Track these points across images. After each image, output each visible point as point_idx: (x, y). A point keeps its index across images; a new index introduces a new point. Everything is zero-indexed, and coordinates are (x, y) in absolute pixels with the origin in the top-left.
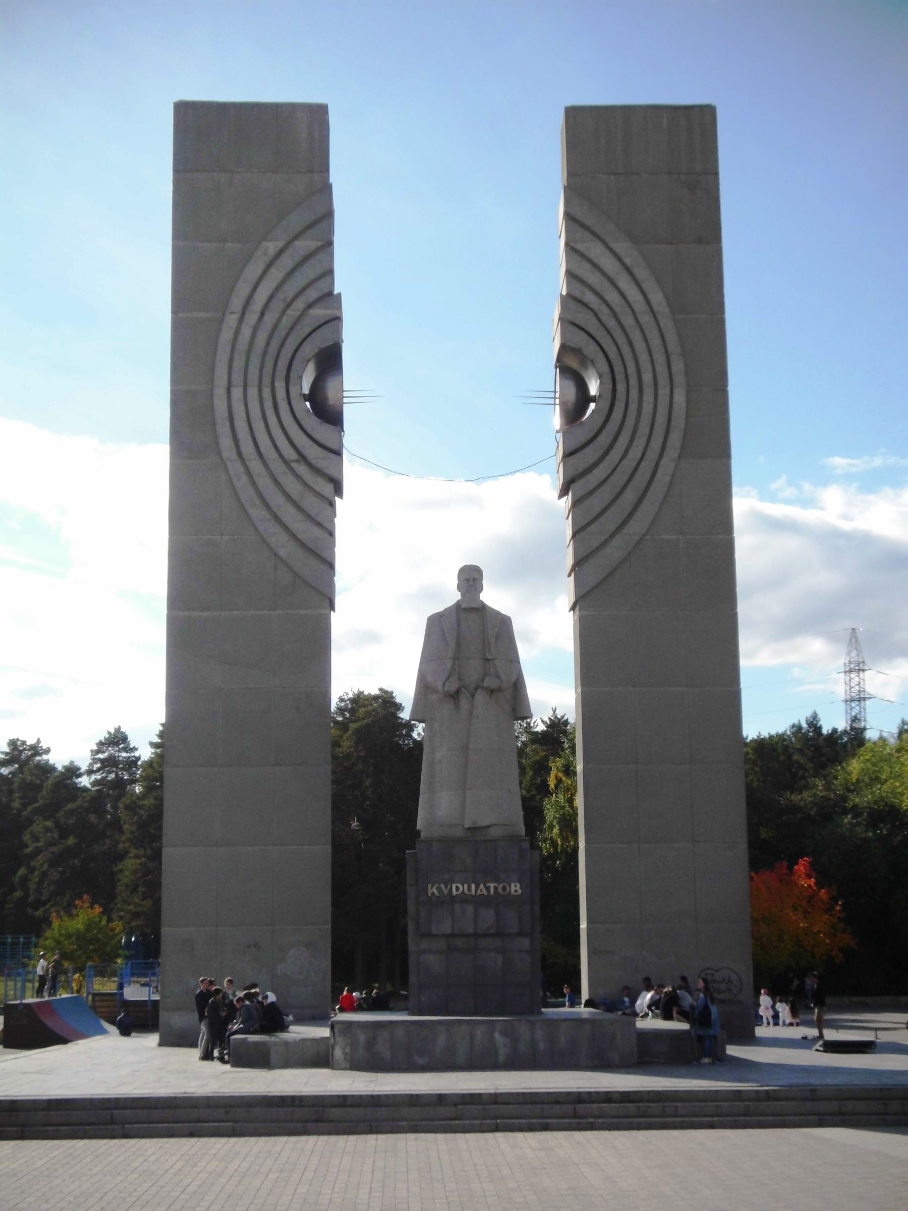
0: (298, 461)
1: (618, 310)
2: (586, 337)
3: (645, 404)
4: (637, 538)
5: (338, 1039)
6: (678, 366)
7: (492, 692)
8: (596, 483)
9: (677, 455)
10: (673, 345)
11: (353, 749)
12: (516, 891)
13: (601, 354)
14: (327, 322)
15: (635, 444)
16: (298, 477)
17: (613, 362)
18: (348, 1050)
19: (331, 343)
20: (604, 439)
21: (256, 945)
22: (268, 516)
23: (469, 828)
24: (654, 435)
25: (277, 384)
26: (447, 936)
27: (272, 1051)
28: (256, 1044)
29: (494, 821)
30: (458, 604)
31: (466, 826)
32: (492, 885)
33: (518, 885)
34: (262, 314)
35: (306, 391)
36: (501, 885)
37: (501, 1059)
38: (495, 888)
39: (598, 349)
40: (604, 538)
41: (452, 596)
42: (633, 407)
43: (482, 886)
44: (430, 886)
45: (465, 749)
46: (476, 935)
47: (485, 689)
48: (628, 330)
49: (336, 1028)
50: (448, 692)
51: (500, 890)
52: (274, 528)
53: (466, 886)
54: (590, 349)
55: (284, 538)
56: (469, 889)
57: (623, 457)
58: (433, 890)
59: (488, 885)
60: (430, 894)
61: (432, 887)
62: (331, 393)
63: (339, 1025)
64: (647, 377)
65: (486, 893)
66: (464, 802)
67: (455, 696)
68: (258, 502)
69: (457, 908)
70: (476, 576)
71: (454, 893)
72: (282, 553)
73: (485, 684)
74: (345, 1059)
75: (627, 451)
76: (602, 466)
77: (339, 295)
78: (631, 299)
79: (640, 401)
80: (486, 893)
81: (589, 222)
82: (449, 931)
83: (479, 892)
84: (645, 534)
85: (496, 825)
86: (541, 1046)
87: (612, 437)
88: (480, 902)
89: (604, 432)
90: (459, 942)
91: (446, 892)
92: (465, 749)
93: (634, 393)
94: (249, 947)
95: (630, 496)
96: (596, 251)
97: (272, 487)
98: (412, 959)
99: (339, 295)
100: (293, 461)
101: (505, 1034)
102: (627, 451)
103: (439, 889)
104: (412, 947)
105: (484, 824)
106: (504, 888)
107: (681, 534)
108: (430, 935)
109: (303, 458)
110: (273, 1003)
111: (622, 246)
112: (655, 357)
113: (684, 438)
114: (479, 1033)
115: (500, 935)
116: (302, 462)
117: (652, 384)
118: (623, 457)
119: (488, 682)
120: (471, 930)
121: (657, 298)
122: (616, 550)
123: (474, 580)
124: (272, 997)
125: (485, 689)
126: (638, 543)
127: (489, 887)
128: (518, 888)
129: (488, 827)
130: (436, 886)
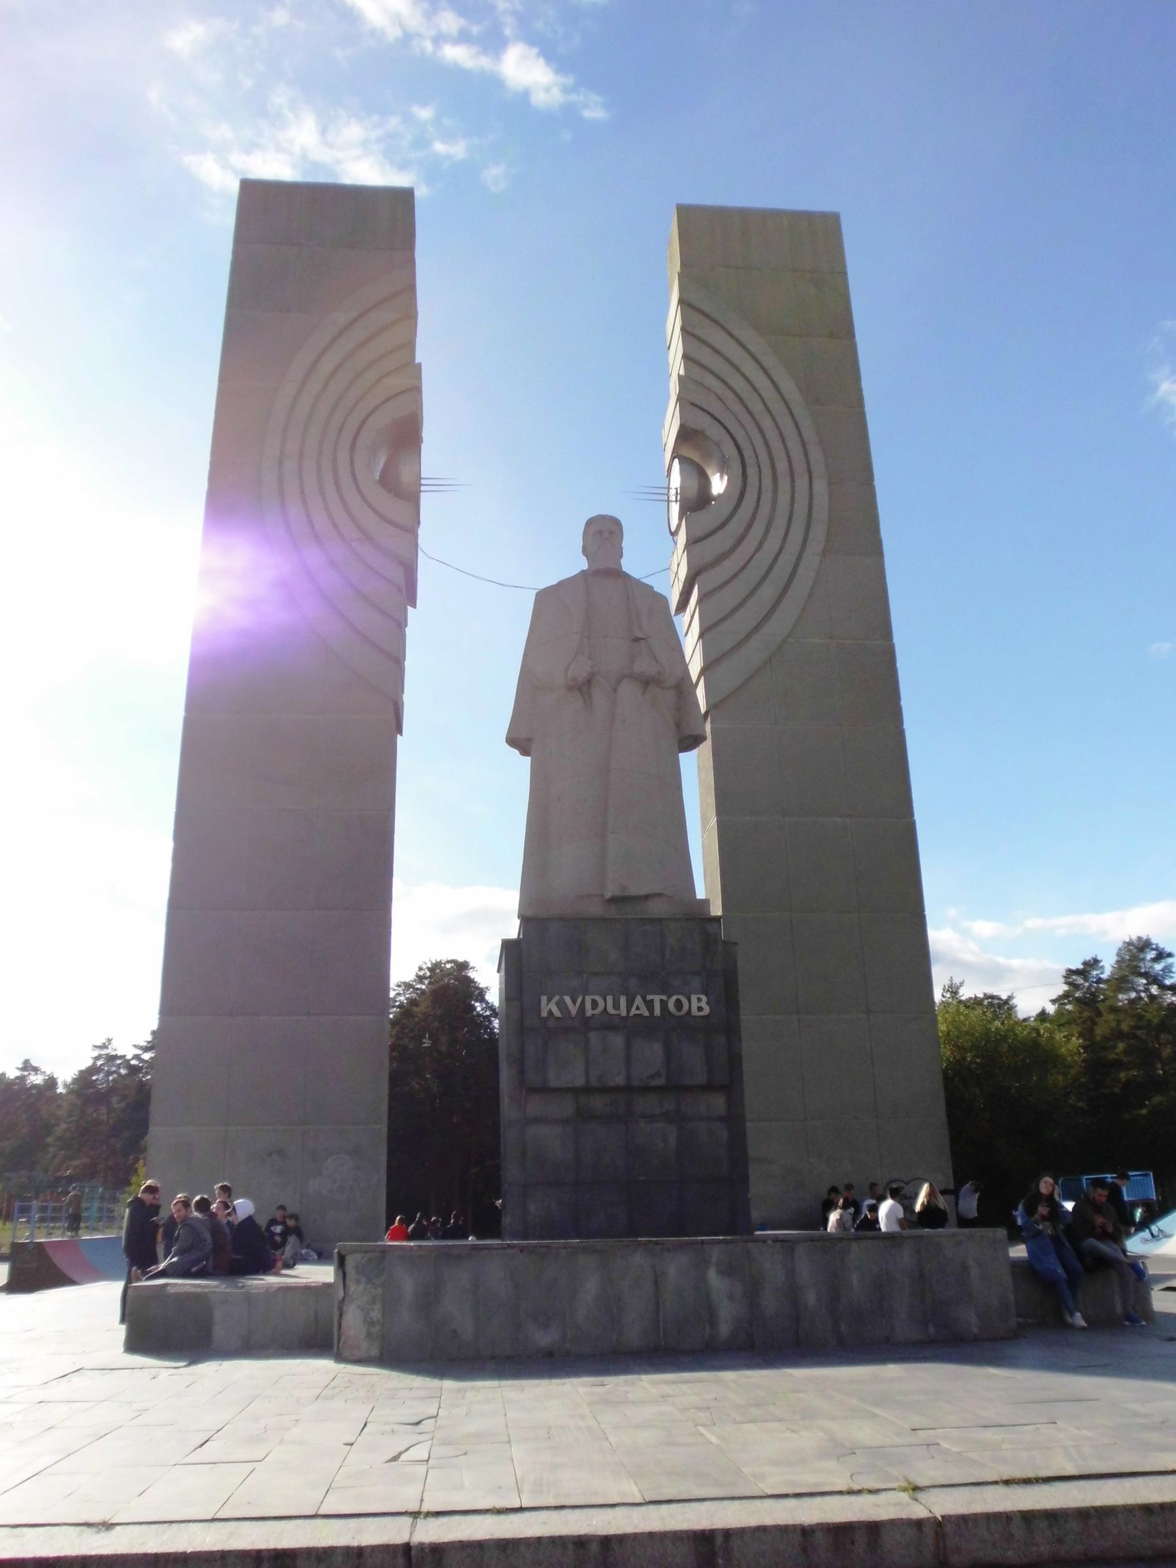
1: (744, 396)
5: (352, 1287)
6: (816, 455)
7: (646, 682)
10: (809, 432)
12: (700, 1009)
13: (727, 437)
14: (404, 392)
17: (742, 446)
18: (376, 1314)
20: (736, 527)
21: (281, 1153)
23: (614, 900)
24: (792, 529)
26: (574, 1091)
27: (218, 1314)
28: (184, 1299)
29: (655, 888)
31: (608, 895)
32: (657, 999)
33: (704, 998)
34: (326, 384)
36: (674, 998)
37: (724, 1329)
38: (664, 1004)
42: (767, 496)
43: (639, 1000)
44: (544, 999)
47: (633, 677)
48: (758, 417)
49: (350, 1262)
53: (610, 999)
54: (714, 431)
56: (616, 1006)
57: (757, 550)
59: (649, 997)
60: (544, 1014)
61: (549, 1000)
62: (405, 476)
63: (358, 1256)
64: (782, 465)
65: (647, 1014)
67: (583, 687)
69: (594, 1037)
71: (589, 1012)
74: (369, 1335)
77: (420, 365)
78: (757, 385)
79: (775, 491)
80: (647, 1014)
81: (706, 308)
82: (580, 1082)
83: (633, 1011)
84: (788, 637)
85: (660, 895)
86: (811, 1298)
88: (638, 1029)
89: (735, 519)
90: (598, 1103)
91: (574, 1010)
93: (767, 481)
94: (270, 1154)
95: (768, 592)
96: (717, 337)
98: (509, 1137)
99: (420, 365)
101: (728, 1270)
103: (561, 1005)
104: (508, 1110)
106: (679, 1004)
108: (544, 1090)
110: (250, 1220)
111: (747, 334)
113: (828, 532)
114: (672, 1271)
115: (674, 1088)
118: (757, 550)
119: (643, 666)
120: (620, 1080)
121: (788, 386)
123: (611, 532)
124: (244, 1207)
125: (633, 677)
128: (703, 1004)
129: (647, 897)
130: (557, 998)
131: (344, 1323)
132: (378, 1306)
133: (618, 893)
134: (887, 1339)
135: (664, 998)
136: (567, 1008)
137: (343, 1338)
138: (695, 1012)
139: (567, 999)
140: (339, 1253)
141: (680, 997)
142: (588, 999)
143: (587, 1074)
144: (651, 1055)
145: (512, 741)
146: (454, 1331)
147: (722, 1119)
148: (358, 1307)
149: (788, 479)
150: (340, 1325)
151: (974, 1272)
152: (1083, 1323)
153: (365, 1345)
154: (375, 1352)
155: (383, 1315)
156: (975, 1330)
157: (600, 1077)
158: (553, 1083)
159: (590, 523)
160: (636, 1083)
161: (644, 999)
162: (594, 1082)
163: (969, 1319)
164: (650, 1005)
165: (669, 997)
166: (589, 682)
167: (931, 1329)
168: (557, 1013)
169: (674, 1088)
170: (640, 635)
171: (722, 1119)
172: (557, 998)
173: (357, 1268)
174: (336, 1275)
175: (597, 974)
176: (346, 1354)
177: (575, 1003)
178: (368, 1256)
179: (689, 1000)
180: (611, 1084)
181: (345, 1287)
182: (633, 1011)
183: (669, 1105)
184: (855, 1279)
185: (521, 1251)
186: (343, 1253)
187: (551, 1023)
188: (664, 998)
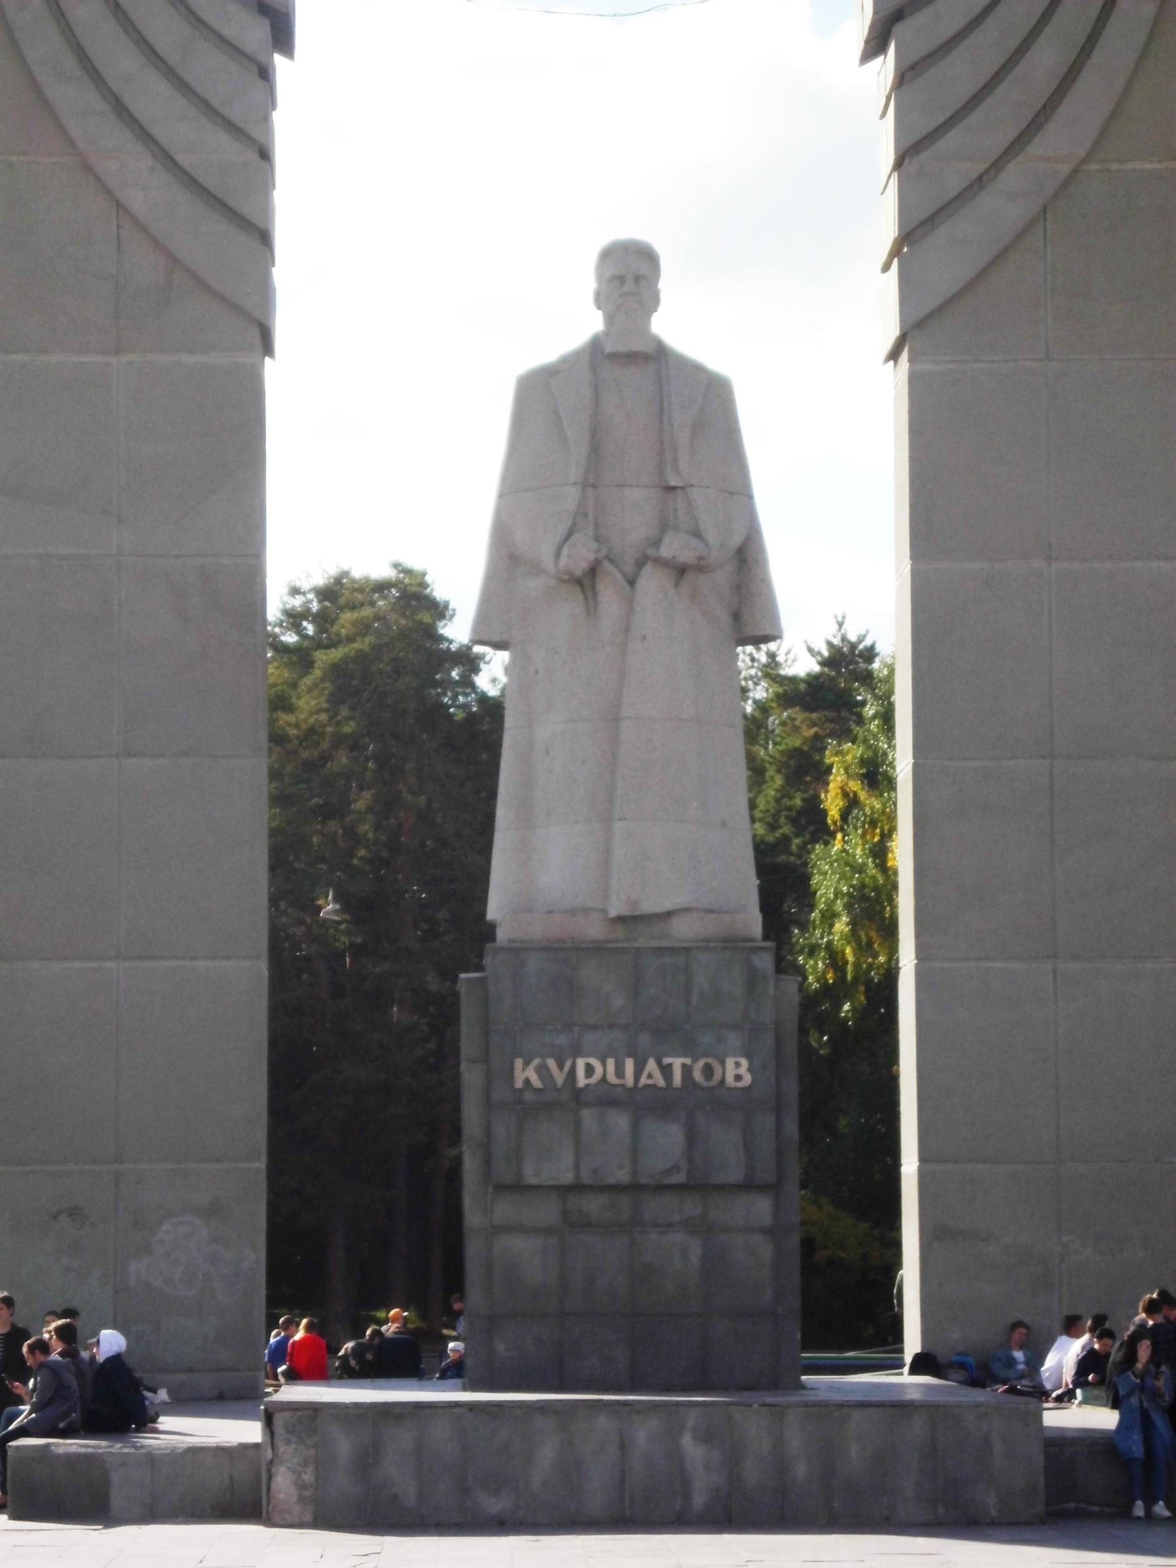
4: (1065, 169)
5: (281, 1448)
8: (959, 22)
11: (324, 717)
12: (738, 1078)
18: (308, 1477)
23: (620, 919)
31: (613, 913)
32: (677, 1063)
36: (701, 1063)
38: (687, 1070)
40: (981, 167)
43: (651, 1065)
44: (519, 1063)
46: (635, 1188)
49: (279, 1420)
50: (568, 572)
51: (697, 1075)
53: (611, 1063)
56: (620, 1072)
58: (526, 1074)
59: (667, 1061)
60: (519, 1084)
61: (527, 1063)
63: (287, 1414)
65: (660, 1082)
67: (585, 582)
69: (588, 1117)
71: (582, 1081)
73: (665, 551)
74: (301, 1499)
80: (660, 1082)
82: (568, 1178)
83: (644, 1080)
84: (1086, 160)
85: (687, 910)
86: (801, 1470)
88: (646, 1104)
90: (593, 1205)
91: (560, 1078)
95: (1048, 57)
98: (473, 1248)
101: (706, 1437)
103: (542, 1071)
106: (708, 1071)
108: (518, 1188)
115: (698, 1186)
119: (675, 547)
120: (622, 1176)
123: (638, 279)
126: (1067, 183)
127: (670, 1065)
129: (668, 915)
130: (536, 1062)
131: (274, 1486)
132: (310, 1469)
133: (625, 911)
134: (888, 1518)
135: (688, 1061)
136: (551, 1076)
137: (273, 1502)
138: (730, 1080)
139: (551, 1063)
140: (266, 1410)
141: (710, 1060)
142: (581, 1063)
143: (577, 1167)
144: (667, 1141)
146: (395, 1496)
147: (766, 1231)
148: (289, 1469)
150: (269, 1489)
151: (998, 1449)
152: (1167, 1513)
153: (297, 1509)
154: (308, 1517)
155: (317, 1478)
156: (994, 1513)
157: (595, 1171)
158: (530, 1179)
160: (644, 1180)
161: (659, 1062)
162: (587, 1179)
163: (991, 1502)
164: (666, 1071)
165: (695, 1061)
166: (593, 571)
167: (941, 1510)
168: (536, 1082)
169: (698, 1186)
170: (673, 483)
171: (766, 1231)
172: (536, 1062)
173: (286, 1427)
174: (264, 1435)
175: (594, 1027)
176: (277, 1519)
177: (561, 1066)
178: (299, 1413)
179: (723, 1063)
180: (611, 1181)
181: (273, 1448)
182: (644, 1080)
183: (691, 1207)
184: (854, 1450)
185: (471, 1410)
186: (270, 1410)
187: (528, 1097)
188: (688, 1061)
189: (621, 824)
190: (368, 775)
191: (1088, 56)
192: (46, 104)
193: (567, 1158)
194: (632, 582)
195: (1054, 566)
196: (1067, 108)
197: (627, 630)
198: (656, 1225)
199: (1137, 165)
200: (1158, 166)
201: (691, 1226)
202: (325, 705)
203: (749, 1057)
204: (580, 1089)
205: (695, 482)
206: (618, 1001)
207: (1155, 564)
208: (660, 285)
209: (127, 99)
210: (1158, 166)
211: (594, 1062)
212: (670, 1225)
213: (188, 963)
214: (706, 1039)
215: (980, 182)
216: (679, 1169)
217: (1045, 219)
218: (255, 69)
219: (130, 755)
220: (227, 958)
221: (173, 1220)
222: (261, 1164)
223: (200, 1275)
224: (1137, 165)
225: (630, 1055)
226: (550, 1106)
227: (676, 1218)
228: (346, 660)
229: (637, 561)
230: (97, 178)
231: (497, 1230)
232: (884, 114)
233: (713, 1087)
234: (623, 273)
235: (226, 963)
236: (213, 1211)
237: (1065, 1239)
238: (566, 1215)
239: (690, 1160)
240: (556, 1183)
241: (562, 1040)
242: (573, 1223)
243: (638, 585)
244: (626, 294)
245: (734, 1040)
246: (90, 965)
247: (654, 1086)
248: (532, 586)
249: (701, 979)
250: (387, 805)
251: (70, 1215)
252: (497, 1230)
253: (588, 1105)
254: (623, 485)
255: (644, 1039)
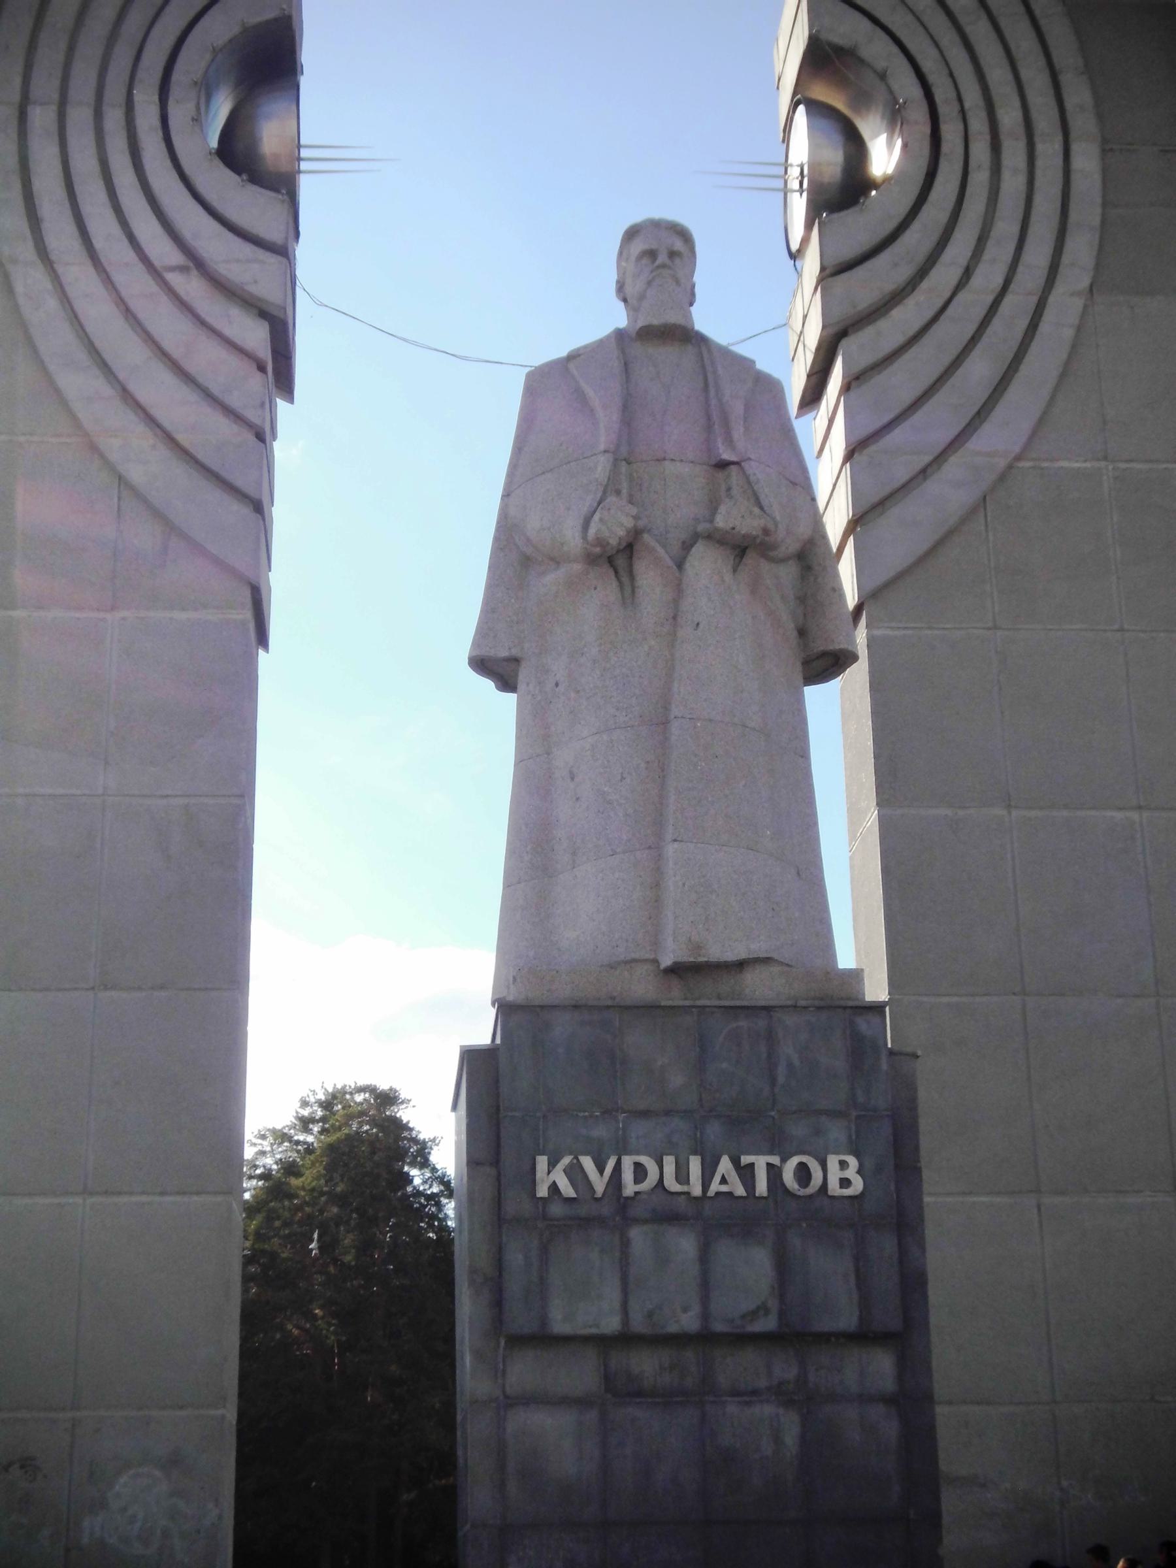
0: (183, 269)
2: (866, 24)
3: (1006, 175)
4: (1002, 463)
9: (1085, 282)
11: (322, 1181)
12: (845, 1183)
15: (987, 256)
16: (185, 306)
17: (932, 78)
19: (269, 15)
20: (918, 239)
22: (107, 391)
23: (677, 971)
25: (139, 96)
26: (603, 1343)
29: (758, 947)
30: (624, 329)
31: (667, 961)
32: (761, 1162)
33: (853, 1161)
35: (214, 144)
36: (794, 1161)
38: (774, 1172)
39: (895, 49)
40: (927, 459)
41: (596, 313)
43: (725, 1165)
44: (542, 1162)
45: (660, 722)
46: (705, 1339)
47: (718, 538)
48: (962, 20)
50: (600, 542)
51: (788, 1176)
52: (120, 417)
55: (141, 438)
56: (682, 1175)
58: (552, 1177)
59: (745, 1160)
60: (542, 1191)
61: (552, 1165)
65: (740, 1191)
66: (657, 885)
67: (618, 559)
68: (82, 356)
69: (636, 1234)
70: (679, 245)
71: (630, 1187)
72: (136, 474)
75: (967, 273)
76: (910, 302)
80: (740, 1191)
82: (611, 1324)
83: (715, 1187)
84: (1018, 458)
85: (767, 961)
87: (935, 237)
89: (916, 226)
90: (646, 1365)
91: (599, 1184)
92: (660, 722)
93: (980, 151)
95: (980, 370)
97: (119, 324)
100: (172, 269)
102: (967, 273)
103: (575, 1173)
104: (471, 1376)
105: (730, 956)
106: (803, 1173)
107: (1105, 458)
108: (543, 1339)
109: (196, 263)
112: (1025, 74)
115: (793, 1337)
116: (195, 272)
117: (1021, 130)
119: (733, 517)
120: (689, 1322)
122: (950, 491)
123: (673, 254)
125: (718, 538)
126: (1002, 478)
127: (751, 1166)
128: (851, 1173)
129: (741, 965)
130: (566, 1160)
133: (685, 957)
135: (775, 1160)
138: (834, 1188)
139: (587, 1163)
142: (628, 1162)
145: (482, 664)
147: (889, 1400)
149: (1022, 145)
157: (650, 1315)
158: (559, 1325)
159: (632, 234)
160: (719, 1327)
161: (736, 1162)
162: (638, 1325)
164: (747, 1173)
165: (784, 1160)
168: (567, 1189)
169: (793, 1337)
170: (727, 456)
171: (889, 1400)
172: (566, 1160)
175: (645, 1114)
177: (601, 1171)
180: (673, 1328)
182: (715, 1187)
183: (785, 1368)
187: (556, 1210)
188: (775, 1160)
189: (676, 845)
190: (353, 1223)
191: (1016, 370)
192: (57, 391)
193: (611, 1294)
194: (680, 565)
195: (1014, 813)
196: (999, 413)
197: (675, 618)
198: (735, 1393)
199: (1065, 464)
200: (1084, 465)
201: (782, 1394)
202: (323, 1172)
203: (857, 1155)
204: (627, 1198)
205: (752, 457)
206: (677, 1080)
207: (1109, 813)
208: (696, 278)
209: (132, 387)
210: (1084, 465)
211: (644, 1160)
212: (755, 1392)
213: (157, 1199)
214: (798, 1130)
215: (924, 473)
216: (767, 1311)
217: (985, 509)
218: (254, 366)
219: (106, 988)
220: (198, 1193)
221: (132, 1472)
222: (230, 1414)
223: (159, 1531)
224: (1065, 464)
225: (695, 1153)
226: (585, 1223)
227: (762, 1383)
228: (339, 1141)
229: (684, 543)
230: (102, 456)
231: (509, 1402)
232: (464, 1419)
233: (811, 1197)
234: (654, 247)
235: (195, 1198)
236: (174, 1462)
237: (1065, 1483)
238: (608, 1378)
239: (782, 1297)
240: (594, 1331)
241: (600, 1131)
242: (621, 1390)
243: (687, 565)
244: (658, 267)
245: (837, 1131)
246: (56, 1201)
247: (730, 1194)
248: (550, 581)
249: (788, 1050)
250: (366, 1246)
251: (22, 1467)
252: (509, 1402)
253: (636, 1221)
254: (664, 459)
255: (714, 1131)
